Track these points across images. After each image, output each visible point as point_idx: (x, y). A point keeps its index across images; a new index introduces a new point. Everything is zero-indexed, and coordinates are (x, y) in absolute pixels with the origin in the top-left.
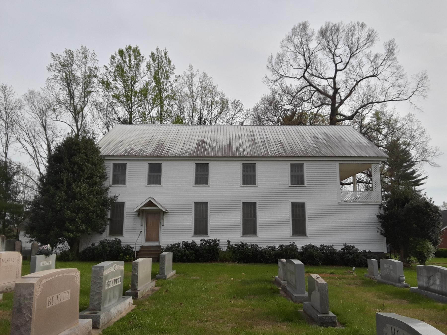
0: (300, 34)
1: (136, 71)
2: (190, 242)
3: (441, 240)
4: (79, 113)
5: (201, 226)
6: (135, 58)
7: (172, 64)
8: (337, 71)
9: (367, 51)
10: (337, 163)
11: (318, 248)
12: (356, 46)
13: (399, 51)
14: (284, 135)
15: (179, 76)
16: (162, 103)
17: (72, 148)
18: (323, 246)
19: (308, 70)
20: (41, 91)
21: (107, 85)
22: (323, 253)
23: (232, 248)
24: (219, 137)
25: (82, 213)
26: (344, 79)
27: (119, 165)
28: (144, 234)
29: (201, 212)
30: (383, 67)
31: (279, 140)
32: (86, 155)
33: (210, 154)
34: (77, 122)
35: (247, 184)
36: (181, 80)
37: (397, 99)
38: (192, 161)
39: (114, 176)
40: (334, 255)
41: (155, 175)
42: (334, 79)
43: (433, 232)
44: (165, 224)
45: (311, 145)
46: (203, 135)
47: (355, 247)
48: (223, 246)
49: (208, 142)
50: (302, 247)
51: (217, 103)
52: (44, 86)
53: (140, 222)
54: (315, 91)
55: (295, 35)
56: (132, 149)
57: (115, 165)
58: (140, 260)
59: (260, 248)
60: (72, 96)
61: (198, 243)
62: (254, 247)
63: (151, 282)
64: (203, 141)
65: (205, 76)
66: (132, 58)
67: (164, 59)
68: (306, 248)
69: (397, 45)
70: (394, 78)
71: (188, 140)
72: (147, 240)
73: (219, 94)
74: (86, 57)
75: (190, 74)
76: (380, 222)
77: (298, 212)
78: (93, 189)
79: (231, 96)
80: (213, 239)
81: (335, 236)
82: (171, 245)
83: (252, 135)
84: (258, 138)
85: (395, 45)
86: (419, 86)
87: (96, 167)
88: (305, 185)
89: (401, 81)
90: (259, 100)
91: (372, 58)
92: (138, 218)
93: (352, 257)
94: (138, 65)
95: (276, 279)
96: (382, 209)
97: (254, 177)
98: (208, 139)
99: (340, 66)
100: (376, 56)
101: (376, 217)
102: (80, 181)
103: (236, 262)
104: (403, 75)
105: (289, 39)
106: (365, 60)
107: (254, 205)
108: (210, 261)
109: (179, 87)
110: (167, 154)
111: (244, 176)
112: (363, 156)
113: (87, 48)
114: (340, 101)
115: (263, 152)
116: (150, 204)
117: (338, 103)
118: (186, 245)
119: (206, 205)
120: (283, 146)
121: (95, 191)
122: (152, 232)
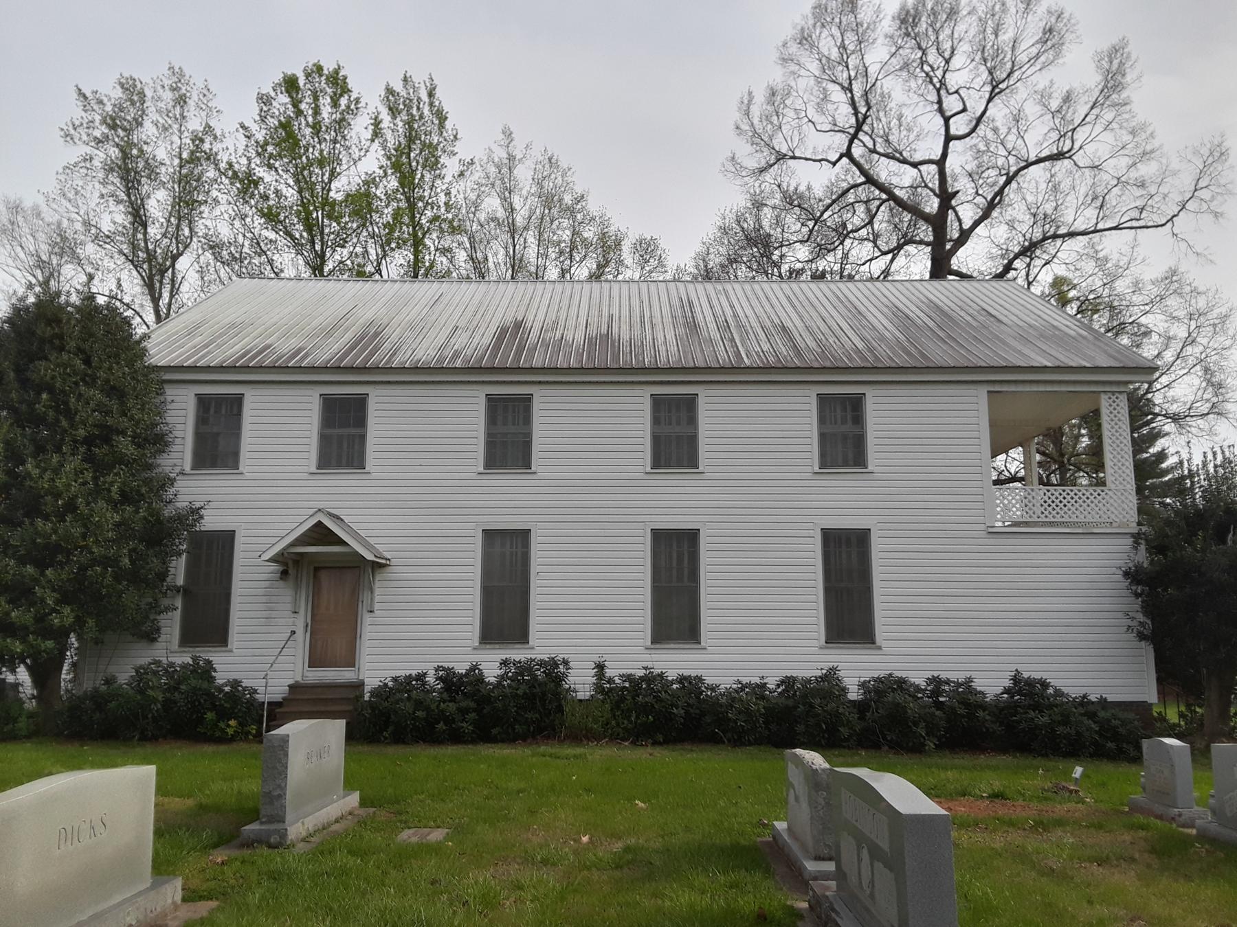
0: (837, 20)
1: (335, 142)
2: (461, 668)
4: (162, 273)
5: (505, 612)
6: (335, 104)
7: (448, 124)
8: (949, 138)
9: (1041, 80)
10: (982, 393)
11: (918, 688)
12: (1009, 65)
13: (1139, 78)
14: (794, 307)
15: (472, 163)
16: (417, 244)
17: (33, 334)
18: (936, 682)
19: (861, 135)
20: (41, 201)
21: (247, 184)
22: (939, 705)
23: (611, 689)
24: (573, 313)
25: (61, 564)
26: (971, 166)
27: (220, 400)
28: (302, 641)
29: (507, 566)
30: (1087, 129)
31: (777, 321)
32: (87, 362)
33: (537, 362)
34: (155, 301)
35: (668, 465)
36: (477, 175)
37: (1135, 224)
38: (475, 387)
39: (200, 437)
40: (980, 713)
42: (941, 163)
44: (377, 606)
45: (887, 334)
46: (523, 309)
47: (1053, 682)
48: (581, 682)
49: (537, 327)
50: (863, 685)
51: (586, 244)
52: (52, 186)
53: (289, 599)
54: (884, 201)
55: (823, 26)
56: (268, 347)
57: (203, 401)
58: (293, 729)
59: (713, 688)
60: (139, 218)
61: (491, 673)
62: (691, 685)
63: (154, 886)
64: (518, 325)
66: (325, 102)
67: (426, 111)
68: (877, 691)
69: (1133, 57)
70: (1124, 162)
71: (470, 322)
72: (313, 663)
73: (593, 219)
74: (182, 100)
75: (505, 156)
76: (1137, 595)
77: (847, 564)
78: (109, 479)
79: (629, 225)
80: (546, 657)
81: (971, 644)
82: (395, 679)
83: (687, 309)
84: (705, 317)
85: (1128, 57)
86: (1201, 184)
87: (122, 403)
88: (870, 468)
89: (1147, 170)
90: (709, 230)
91: (1054, 105)
92: (281, 583)
93: (1046, 719)
94: (341, 124)
95: (776, 836)
96: (1143, 547)
97: (693, 440)
98: (536, 319)
99: (959, 125)
100: (1067, 99)
101: (1120, 577)
102: (58, 449)
103: (624, 739)
104: (1152, 152)
105: (804, 39)
106: (1032, 110)
107: (692, 536)
108: (534, 737)
109: (473, 196)
110: (387, 362)
111: (657, 440)
112: (1074, 364)
113: (187, 72)
114: (956, 235)
115: (723, 356)
116: (320, 534)
117: (951, 240)
118: (449, 680)
120: (791, 338)
121: (115, 488)
122: (333, 637)
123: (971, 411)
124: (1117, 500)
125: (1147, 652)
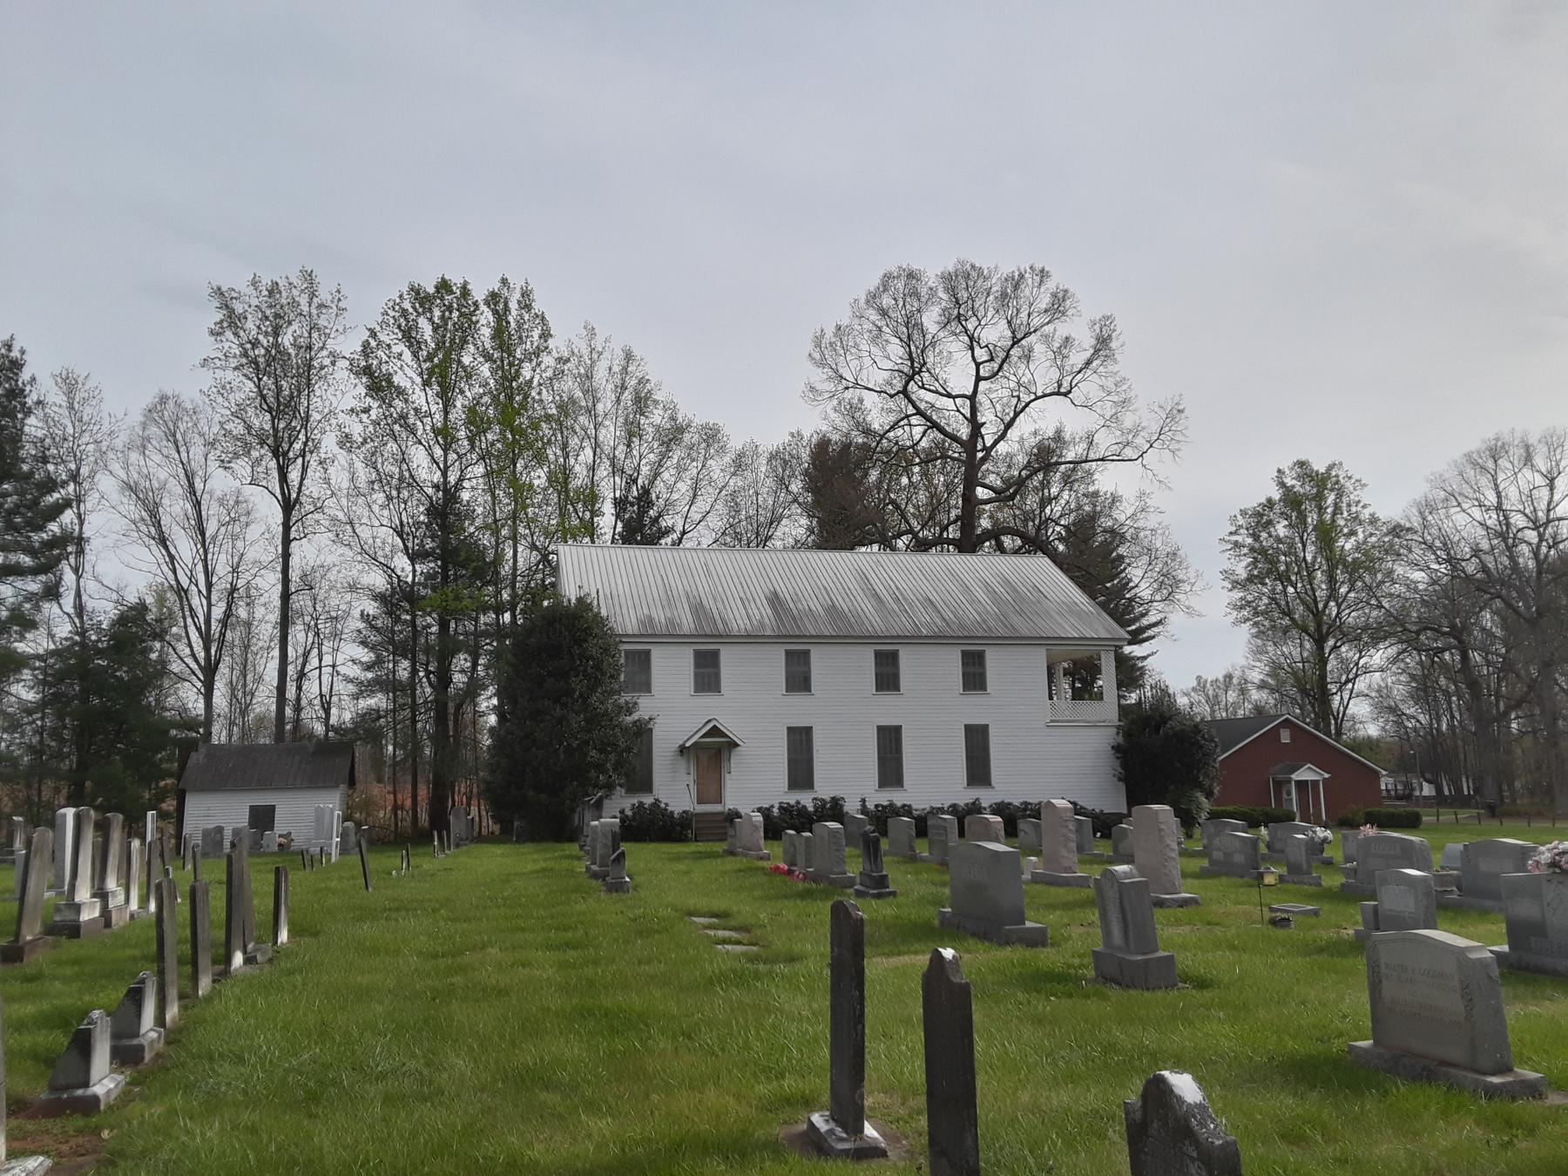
3: (483, 706)
8: (978, 379)
18: (1026, 804)
27: (640, 652)
28: (694, 789)
41: (707, 675)
43: (1206, 775)
65: (629, 357)
119: (808, 731)
122: (710, 786)
123: (1038, 660)
124: (1107, 710)
125: (1122, 786)
